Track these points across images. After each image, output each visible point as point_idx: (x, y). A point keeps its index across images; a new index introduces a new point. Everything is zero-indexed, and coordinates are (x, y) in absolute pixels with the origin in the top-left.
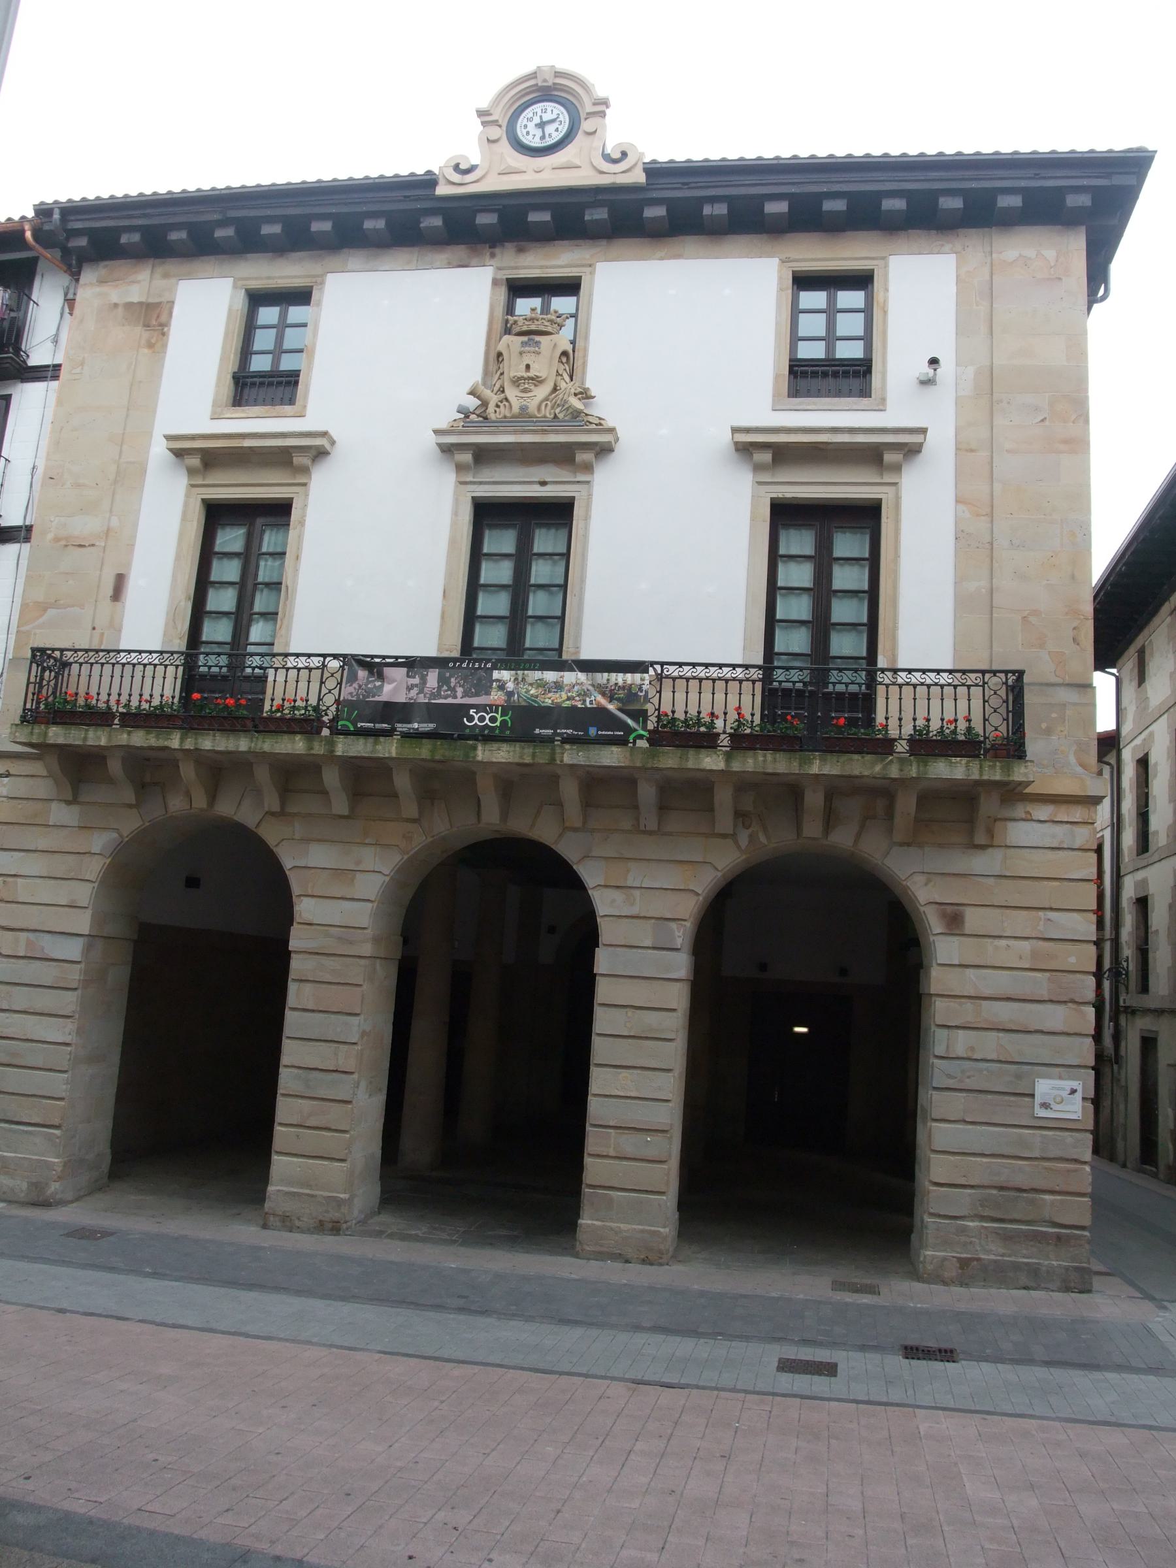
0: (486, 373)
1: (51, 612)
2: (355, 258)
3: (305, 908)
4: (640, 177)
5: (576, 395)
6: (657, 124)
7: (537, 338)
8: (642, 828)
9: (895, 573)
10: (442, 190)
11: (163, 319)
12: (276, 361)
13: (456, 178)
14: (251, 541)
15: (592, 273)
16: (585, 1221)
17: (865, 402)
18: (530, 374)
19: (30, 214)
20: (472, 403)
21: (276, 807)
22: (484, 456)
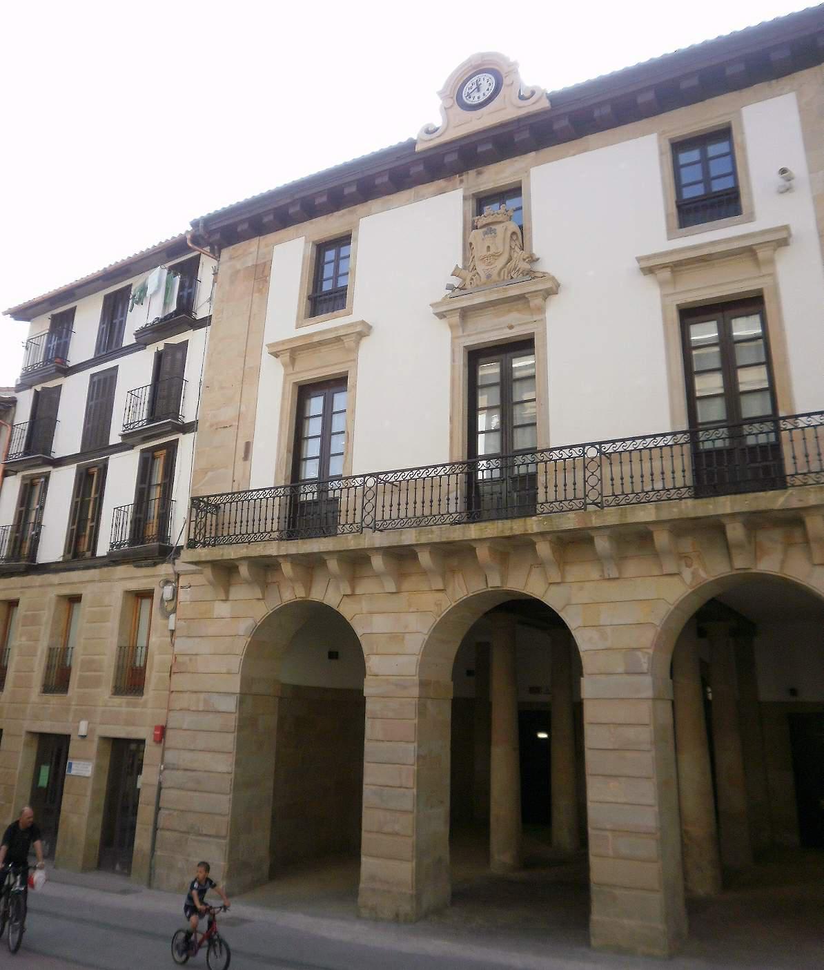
0: (465, 259)
1: (210, 474)
2: (374, 204)
3: (373, 663)
4: (545, 104)
5: (524, 260)
6: (554, 67)
7: (493, 227)
8: (606, 576)
9: (463, 446)
10: (418, 148)
11: (266, 273)
12: (336, 282)
13: (428, 137)
14: (328, 405)
15: (528, 176)
16: (595, 917)
17: (738, 218)
18: (490, 253)
19: (190, 228)
20: (456, 282)
21: (349, 592)
22: (465, 313)
